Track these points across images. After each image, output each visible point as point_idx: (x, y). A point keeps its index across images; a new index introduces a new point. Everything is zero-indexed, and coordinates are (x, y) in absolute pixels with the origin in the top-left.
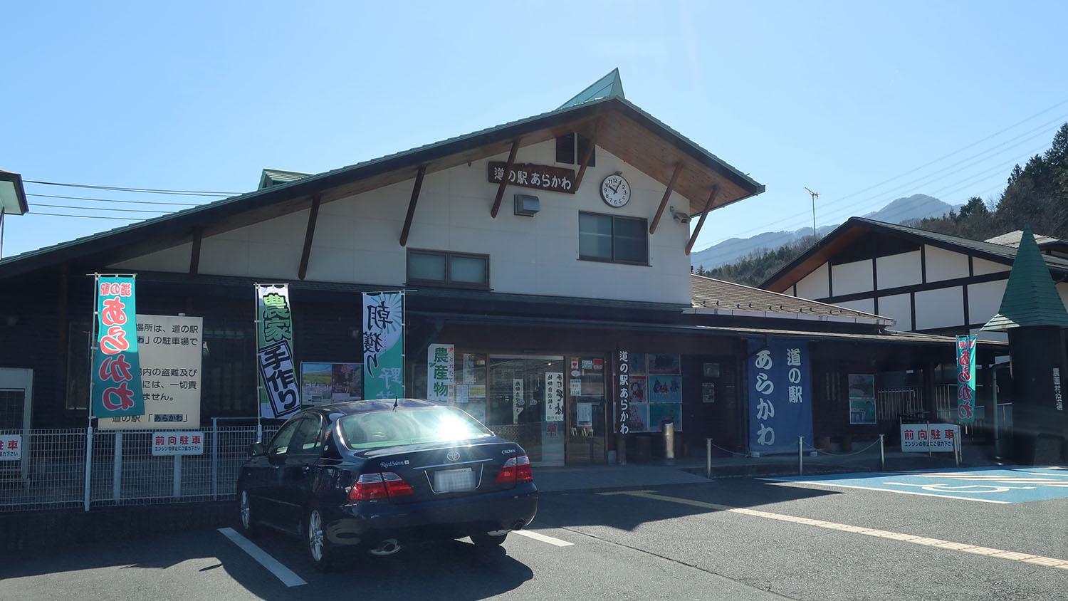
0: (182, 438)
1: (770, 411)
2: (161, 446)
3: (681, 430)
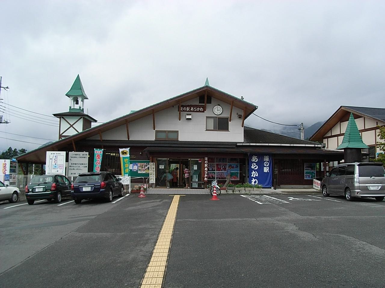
1: (256, 174)
3: (239, 180)
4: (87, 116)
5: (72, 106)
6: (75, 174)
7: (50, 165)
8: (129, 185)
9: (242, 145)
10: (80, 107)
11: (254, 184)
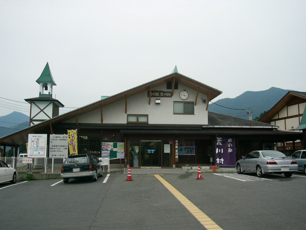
0: (28, 160)
2: (24, 161)
4: (57, 101)
5: (41, 92)
6: (56, 155)
7: (32, 147)
8: (108, 165)
9: (231, 128)
10: (49, 93)
11: (105, 172)
